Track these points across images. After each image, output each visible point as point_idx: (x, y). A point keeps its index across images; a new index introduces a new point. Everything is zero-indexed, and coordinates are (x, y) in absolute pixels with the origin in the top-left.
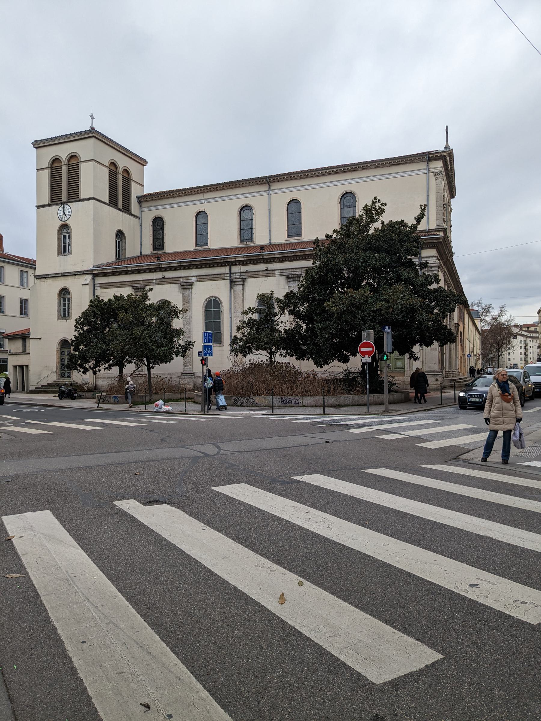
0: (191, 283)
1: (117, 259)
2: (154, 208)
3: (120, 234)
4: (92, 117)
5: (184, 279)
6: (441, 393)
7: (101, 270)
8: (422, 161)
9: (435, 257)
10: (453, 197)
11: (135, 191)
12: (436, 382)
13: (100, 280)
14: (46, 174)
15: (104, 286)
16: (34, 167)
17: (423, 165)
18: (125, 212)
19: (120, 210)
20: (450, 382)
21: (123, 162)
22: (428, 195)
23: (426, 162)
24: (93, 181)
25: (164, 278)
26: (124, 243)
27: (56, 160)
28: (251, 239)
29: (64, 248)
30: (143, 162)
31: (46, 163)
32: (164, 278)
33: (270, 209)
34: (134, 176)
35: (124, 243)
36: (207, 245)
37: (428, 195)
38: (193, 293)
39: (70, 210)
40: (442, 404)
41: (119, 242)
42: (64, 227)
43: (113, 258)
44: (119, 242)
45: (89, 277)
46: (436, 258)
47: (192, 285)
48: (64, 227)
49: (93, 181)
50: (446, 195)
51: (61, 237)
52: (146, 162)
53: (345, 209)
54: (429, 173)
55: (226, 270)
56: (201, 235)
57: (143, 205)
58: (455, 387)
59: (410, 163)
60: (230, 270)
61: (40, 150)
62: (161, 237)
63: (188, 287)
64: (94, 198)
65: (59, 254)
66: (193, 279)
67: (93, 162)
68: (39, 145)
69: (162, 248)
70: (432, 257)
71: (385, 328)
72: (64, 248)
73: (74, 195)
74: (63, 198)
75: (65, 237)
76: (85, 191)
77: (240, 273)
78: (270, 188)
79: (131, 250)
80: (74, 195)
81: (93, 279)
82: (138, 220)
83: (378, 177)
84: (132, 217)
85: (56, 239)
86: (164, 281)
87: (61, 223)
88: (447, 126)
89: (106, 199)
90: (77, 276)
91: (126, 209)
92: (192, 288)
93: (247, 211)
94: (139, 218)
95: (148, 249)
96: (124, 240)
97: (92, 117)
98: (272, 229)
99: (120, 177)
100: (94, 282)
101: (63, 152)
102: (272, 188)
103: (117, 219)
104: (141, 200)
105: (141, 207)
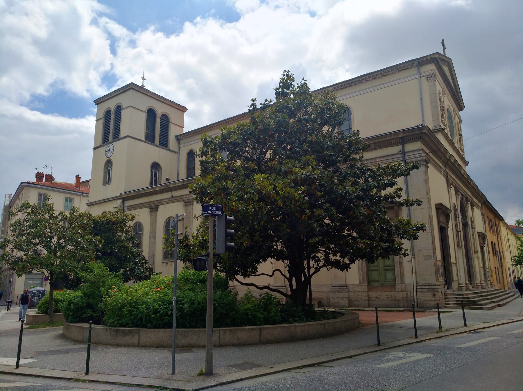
2: (189, 144)
3: (156, 166)
4: (143, 79)
6: (439, 312)
7: (500, 253)
8: (413, 67)
9: (420, 150)
10: (462, 110)
11: (173, 132)
12: (433, 298)
13: (128, 203)
14: (102, 122)
17: (414, 71)
19: (157, 146)
20: (456, 298)
21: (160, 109)
22: (421, 99)
23: (417, 68)
24: (133, 123)
25: (172, 197)
29: (107, 180)
30: (183, 109)
31: (102, 115)
32: (172, 197)
37: (421, 99)
38: (194, 209)
40: (379, 344)
42: (109, 163)
45: (120, 201)
46: (421, 152)
48: (109, 163)
49: (133, 123)
50: (448, 102)
52: (187, 109)
54: (421, 77)
57: (181, 142)
58: (462, 304)
59: (401, 71)
63: (189, 203)
64: (128, 136)
67: (130, 108)
70: (417, 150)
72: (107, 180)
73: (117, 137)
75: (109, 170)
80: (117, 137)
81: (123, 202)
82: (175, 156)
83: (371, 89)
84: (169, 152)
85: (103, 172)
86: (173, 200)
87: (107, 159)
88: (443, 40)
89: (143, 137)
90: (113, 201)
91: (164, 144)
94: (178, 153)
96: (160, 171)
97: (143, 79)
99: (158, 121)
100: (124, 205)
101: (111, 105)
103: (155, 153)
104: (178, 138)
105: (179, 144)
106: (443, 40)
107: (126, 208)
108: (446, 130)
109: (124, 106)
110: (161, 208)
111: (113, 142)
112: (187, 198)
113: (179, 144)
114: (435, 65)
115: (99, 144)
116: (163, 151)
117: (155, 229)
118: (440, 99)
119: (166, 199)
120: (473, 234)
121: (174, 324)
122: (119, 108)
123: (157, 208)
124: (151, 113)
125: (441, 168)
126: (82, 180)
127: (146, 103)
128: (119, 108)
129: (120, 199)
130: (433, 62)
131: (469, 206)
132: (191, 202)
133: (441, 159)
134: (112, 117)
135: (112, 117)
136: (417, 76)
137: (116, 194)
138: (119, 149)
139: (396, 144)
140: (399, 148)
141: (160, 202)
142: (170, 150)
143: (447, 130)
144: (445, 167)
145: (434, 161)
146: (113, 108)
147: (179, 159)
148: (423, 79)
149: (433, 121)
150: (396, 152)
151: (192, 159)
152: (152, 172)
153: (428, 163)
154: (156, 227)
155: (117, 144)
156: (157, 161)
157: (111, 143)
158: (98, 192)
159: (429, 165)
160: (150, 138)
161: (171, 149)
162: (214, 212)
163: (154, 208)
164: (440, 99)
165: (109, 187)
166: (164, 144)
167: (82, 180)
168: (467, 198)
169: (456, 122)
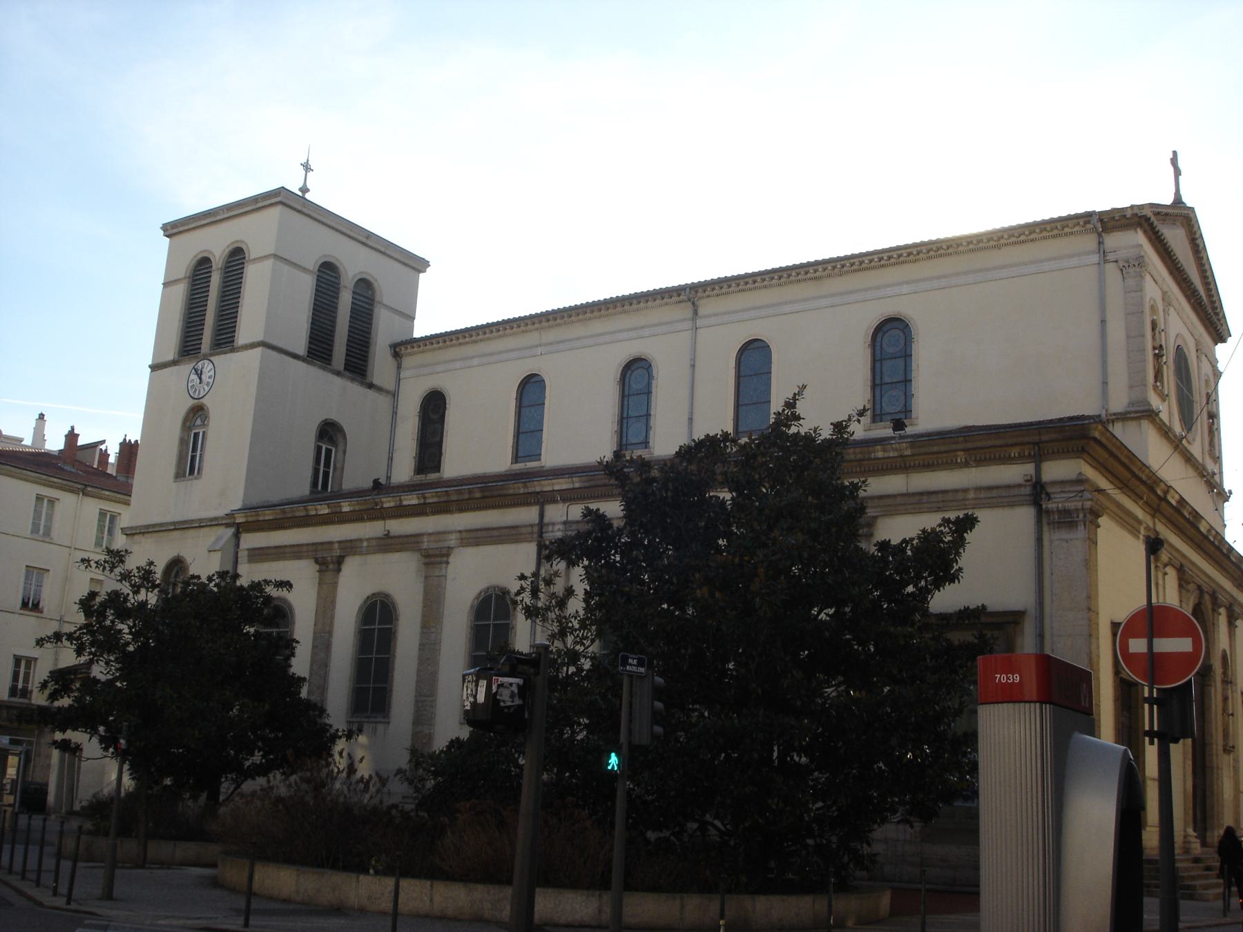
0: (444, 551)
1: (312, 492)
3: (329, 432)
4: (307, 167)
5: (432, 538)
10: (1223, 340)
11: (384, 332)
13: (250, 540)
14: (181, 291)
15: (259, 555)
16: (161, 280)
18: (353, 380)
19: (338, 373)
21: (354, 263)
22: (1103, 322)
25: (388, 535)
26: (340, 454)
27: (203, 264)
28: (646, 444)
29: (189, 464)
31: (183, 269)
32: (388, 535)
33: (693, 366)
34: (386, 292)
35: (340, 454)
36: (537, 457)
37: (1103, 322)
39: (212, 373)
41: (329, 452)
42: (197, 412)
43: (304, 489)
44: (329, 452)
47: (448, 555)
48: (197, 412)
49: (272, 305)
51: (189, 436)
53: (884, 363)
54: (1106, 261)
55: (529, 515)
56: (527, 432)
57: (407, 362)
60: (542, 515)
61: (176, 238)
62: (437, 439)
63: (438, 559)
64: (275, 256)
65: (179, 475)
66: (452, 540)
68: (173, 230)
69: (437, 468)
71: (625, 662)
72: (189, 464)
73: (225, 340)
74: (203, 346)
75: (196, 435)
76: (250, 326)
77: (565, 523)
78: (695, 313)
79: (356, 471)
80: (225, 340)
81: (237, 536)
86: (388, 544)
87: (191, 402)
88: (1175, 153)
92: (448, 563)
93: (640, 371)
94: (394, 395)
95: (404, 471)
96: (341, 447)
97: (307, 167)
98: (695, 417)
100: (237, 546)
101: (216, 243)
102: (701, 311)
103: (330, 394)
106: (1175, 153)
107: (243, 555)
108: (1161, 415)
109: (253, 252)
110: (351, 566)
111: (212, 355)
112: (433, 545)
113: (399, 367)
114: (1145, 232)
115: (170, 356)
116: (354, 389)
117: (332, 624)
118: (1154, 325)
119: (368, 540)
120: (1225, 699)
121: (617, 877)
122: (237, 256)
123: (340, 561)
124: (328, 274)
125: (1140, 522)
126: (81, 442)
127: (318, 246)
128: (237, 256)
129: (227, 525)
130: (1140, 225)
131: (1222, 620)
132: (442, 556)
133: (1142, 498)
134: (216, 280)
135: (216, 280)
136: (1095, 258)
137: (221, 512)
138: (234, 380)
139: (1021, 459)
140: (1029, 468)
141: (350, 547)
142: (371, 386)
143: (1168, 411)
144: (1153, 516)
145: (1119, 506)
146: (218, 255)
147: (395, 413)
148: (1111, 269)
149: (1131, 387)
150: (1020, 480)
151: (435, 417)
152: (319, 449)
153: (1098, 516)
154: (332, 617)
155: (226, 363)
156: (334, 416)
157: (206, 357)
158: (155, 494)
159: (1101, 521)
160: (318, 349)
161: (376, 381)
162: (634, 669)
163: (329, 562)
164: (1154, 325)
165: (197, 487)
166: (357, 366)
167: (81, 442)
168: (1214, 596)
169: (1203, 378)
